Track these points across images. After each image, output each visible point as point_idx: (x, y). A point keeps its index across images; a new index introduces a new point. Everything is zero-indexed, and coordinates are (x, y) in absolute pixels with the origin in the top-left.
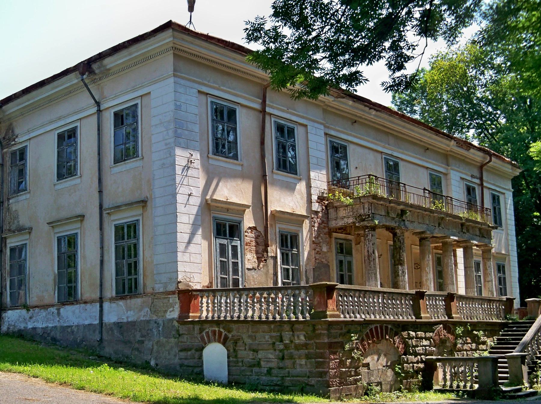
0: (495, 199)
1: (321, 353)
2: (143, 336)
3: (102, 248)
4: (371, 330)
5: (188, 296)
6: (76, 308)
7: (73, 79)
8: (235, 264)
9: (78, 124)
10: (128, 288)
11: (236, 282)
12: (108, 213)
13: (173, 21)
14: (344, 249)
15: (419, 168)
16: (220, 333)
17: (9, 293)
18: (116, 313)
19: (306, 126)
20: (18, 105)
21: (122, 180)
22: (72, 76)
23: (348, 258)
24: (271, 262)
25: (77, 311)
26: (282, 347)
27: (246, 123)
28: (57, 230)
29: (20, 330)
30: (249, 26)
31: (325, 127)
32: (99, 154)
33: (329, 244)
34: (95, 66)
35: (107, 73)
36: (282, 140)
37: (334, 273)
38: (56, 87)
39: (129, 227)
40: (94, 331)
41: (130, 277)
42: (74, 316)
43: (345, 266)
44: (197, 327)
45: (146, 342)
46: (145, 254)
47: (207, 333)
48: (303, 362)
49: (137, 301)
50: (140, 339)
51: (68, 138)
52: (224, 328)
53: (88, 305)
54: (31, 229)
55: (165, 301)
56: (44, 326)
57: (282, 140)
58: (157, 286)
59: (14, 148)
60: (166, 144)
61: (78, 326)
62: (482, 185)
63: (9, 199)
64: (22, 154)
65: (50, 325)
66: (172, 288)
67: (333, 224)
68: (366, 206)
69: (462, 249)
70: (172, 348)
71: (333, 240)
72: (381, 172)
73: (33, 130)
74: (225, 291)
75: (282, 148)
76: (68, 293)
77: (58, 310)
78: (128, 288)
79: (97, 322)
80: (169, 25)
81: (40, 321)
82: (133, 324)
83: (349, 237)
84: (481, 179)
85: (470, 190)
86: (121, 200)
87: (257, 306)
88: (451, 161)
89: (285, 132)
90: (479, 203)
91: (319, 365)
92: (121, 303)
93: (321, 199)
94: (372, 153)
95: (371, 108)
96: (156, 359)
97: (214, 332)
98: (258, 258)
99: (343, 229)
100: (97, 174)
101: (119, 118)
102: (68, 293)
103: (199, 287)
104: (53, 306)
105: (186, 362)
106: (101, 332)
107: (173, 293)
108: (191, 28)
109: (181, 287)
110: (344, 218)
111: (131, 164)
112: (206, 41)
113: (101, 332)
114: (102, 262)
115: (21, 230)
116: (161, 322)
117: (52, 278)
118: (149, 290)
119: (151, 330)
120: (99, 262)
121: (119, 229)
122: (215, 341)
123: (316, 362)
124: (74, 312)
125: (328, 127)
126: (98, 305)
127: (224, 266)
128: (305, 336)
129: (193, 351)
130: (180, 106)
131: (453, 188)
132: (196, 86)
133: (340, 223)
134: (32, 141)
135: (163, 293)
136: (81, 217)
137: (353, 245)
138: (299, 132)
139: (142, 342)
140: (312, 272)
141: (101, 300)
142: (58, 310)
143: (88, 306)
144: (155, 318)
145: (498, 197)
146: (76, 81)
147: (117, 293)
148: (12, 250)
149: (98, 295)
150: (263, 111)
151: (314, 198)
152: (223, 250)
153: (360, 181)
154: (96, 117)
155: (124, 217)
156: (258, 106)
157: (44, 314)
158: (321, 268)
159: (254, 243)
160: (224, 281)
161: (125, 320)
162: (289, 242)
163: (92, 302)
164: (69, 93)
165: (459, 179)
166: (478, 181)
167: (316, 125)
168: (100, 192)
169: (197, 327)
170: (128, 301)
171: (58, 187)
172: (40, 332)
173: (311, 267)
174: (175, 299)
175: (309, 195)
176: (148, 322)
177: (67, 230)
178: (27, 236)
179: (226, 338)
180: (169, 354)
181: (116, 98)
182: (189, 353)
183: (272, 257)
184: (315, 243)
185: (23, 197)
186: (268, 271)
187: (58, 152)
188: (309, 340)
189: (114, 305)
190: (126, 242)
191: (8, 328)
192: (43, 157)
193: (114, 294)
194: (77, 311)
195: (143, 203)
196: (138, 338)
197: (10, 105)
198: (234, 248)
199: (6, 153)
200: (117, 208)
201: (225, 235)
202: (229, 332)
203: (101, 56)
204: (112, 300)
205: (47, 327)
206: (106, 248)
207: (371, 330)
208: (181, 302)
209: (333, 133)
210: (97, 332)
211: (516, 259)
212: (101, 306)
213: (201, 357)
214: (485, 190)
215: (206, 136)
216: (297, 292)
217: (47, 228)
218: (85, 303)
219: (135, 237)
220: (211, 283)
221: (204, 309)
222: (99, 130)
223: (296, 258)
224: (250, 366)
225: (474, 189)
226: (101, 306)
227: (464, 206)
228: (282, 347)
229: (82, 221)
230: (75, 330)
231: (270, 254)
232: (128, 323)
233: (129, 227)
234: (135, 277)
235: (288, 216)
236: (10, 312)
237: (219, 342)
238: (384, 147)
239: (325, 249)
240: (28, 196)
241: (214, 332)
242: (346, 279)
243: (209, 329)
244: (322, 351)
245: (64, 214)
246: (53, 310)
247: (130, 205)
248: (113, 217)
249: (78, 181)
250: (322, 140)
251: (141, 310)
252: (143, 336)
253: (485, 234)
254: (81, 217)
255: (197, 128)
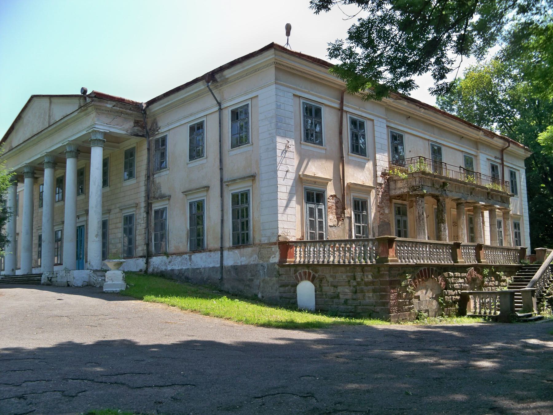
0: (513, 175)
1: (384, 288)
2: (252, 276)
3: (222, 210)
4: (421, 271)
5: (285, 247)
6: (203, 255)
7: (201, 86)
8: (321, 223)
9: (204, 119)
10: (242, 239)
11: (321, 236)
12: (227, 185)
13: (275, 43)
14: (401, 212)
15: (457, 152)
16: (310, 274)
17: (153, 244)
18: (232, 258)
19: (373, 120)
20: (160, 105)
21: (237, 160)
22: (200, 83)
23: (404, 218)
24: (347, 221)
25: (204, 257)
26: (355, 284)
27: (328, 119)
28: (189, 197)
29: (162, 272)
30: (330, 47)
31: (387, 121)
32: (220, 141)
33: (390, 207)
34: (217, 76)
35: (226, 81)
36: (355, 131)
37: (394, 229)
38: (188, 92)
39: (242, 195)
40: (217, 272)
41: (243, 232)
42: (203, 261)
43: (402, 224)
44: (292, 269)
45: (255, 280)
46: (256, 215)
47: (300, 273)
48: (371, 295)
49: (249, 250)
50: (251, 278)
51: (197, 129)
52: (312, 270)
53: (212, 253)
54: (170, 196)
55: (269, 250)
56: (180, 268)
57: (355, 131)
58: (263, 239)
59: (158, 137)
60: (270, 134)
61: (204, 268)
62: (502, 164)
63: (153, 175)
64: (163, 141)
65: (184, 268)
66: (274, 240)
67: (393, 193)
68: (417, 180)
69: (488, 212)
70: (274, 284)
71: (393, 204)
72: (428, 155)
73: (172, 124)
74: (313, 242)
75: (355, 137)
76: (197, 243)
77: (190, 256)
78: (242, 239)
79: (218, 265)
80: (272, 46)
81: (177, 265)
82: (245, 267)
83: (405, 202)
84: (502, 160)
85: (494, 168)
86: (236, 175)
87: (337, 253)
88: (480, 146)
89: (357, 125)
90: (500, 178)
91: (382, 297)
92: (237, 251)
93: (384, 174)
94: (421, 140)
95: (421, 107)
96: (262, 293)
97: (305, 273)
98: (337, 218)
99: (400, 197)
100: (219, 156)
101: (235, 115)
102: (197, 243)
103: (293, 239)
104: (186, 253)
105: (284, 295)
106: (222, 273)
107: (275, 244)
108: (288, 48)
109: (281, 239)
110: (401, 188)
111: (243, 149)
112: (299, 57)
113: (222, 273)
114: (222, 221)
115: (162, 197)
116: (266, 265)
117: (186, 232)
118: (257, 241)
119: (259, 271)
120: (220, 221)
121: (235, 197)
122: (306, 279)
123: (381, 295)
124: (201, 258)
125: (389, 121)
126: (219, 252)
127: (312, 224)
128: (372, 276)
129: (290, 287)
130: (280, 105)
131: (482, 166)
132: (292, 91)
133: (398, 192)
134: (170, 132)
135: (267, 244)
136: (207, 188)
137: (408, 208)
138: (368, 125)
139: (252, 280)
140: (377, 228)
141: (222, 249)
142: (190, 256)
143: (212, 254)
144: (261, 262)
145: (515, 173)
146: (203, 87)
147: (233, 244)
148: (156, 212)
149: (220, 245)
150: (341, 110)
151: (379, 173)
152: (311, 212)
153: (413, 161)
154: (218, 114)
155: (239, 188)
156: (337, 106)
157: (180, 259)
158: (383, 226)
159: (334, 207)
160: (312, 235)
161: (239, 264)
162: (360, 206)
163: (215, 250)
164: (198, 96)
165: (485, 160)
166: (499, 161)
167: (380, 120)
168: (221, 169)
169: (292, 269)
170: (242, 250)
171: (190, 165)
172: (176, 272)
173: (376, 225)
174: (276, 249)
175: (375, 171)
176: (256, 265)
177: (196, 197)
178: (167, 202)
179: (314, 277)
180: (272, 289)
181: (233, 98)
182: (287, 288)
183: (347, 217)
184: (379, 207)
185: (164, 173)
186: (345, 227)
187: (190, 140)
188: (375, 278)
189: (231, 253)
190: (240, 207)
191: (153, 270)
192: (178, 144)
193: (231, 245)
194: (204, 257)
195: (253, 177)
196: (249, 277)
197: (155, 105)
198: (320, 211)
199: (151, 140)
200: (234, 181)
201: (313, 201)
202: (316, 272)
203: (221, 69)
204: (230, 249)
205: (182, 269)
206: (225, 211)
207: (421, 271)
208: (281, 250)
209: (392, 125)
210: (219, 273)
211: (528, 219)
212: (222, 254)
213: (295, 291)
214: (505, 168)
215: (299, 127)
216: (366, 243)
217: (182, 195)
218: (210, 251)
219: (247, 203)
220: (303, 236)
221: (298, 255)
222: (220, 123)
223: (365, 219)
224: (332, 298)
225: (497, 167)
226: (222, 254)
227: (489, 179)
228: (355, 284)
229: (207, 191)
230: (203, 271)
231: (346, 215)
232: (242, 266)
233: (242, 195)
234: (247, 232)
235: (360, 187)
236: (154, 258)
237: (309, 280)
238: (430, 136)
239: (387, 211)
240: (168, 172)
241: (305, 273)
242: (402, 233)
243: (301, 271)
244: (384, 287)
245: (194, 186)
246: (186, 256)
247: (243, 179)
248: (231, 188)
249: (205, 161)
250: (385, 131)
251: (251, 257)
252: (252, 276)
253: (504, 200)
254: (207, 188)
255: (292, 122)
